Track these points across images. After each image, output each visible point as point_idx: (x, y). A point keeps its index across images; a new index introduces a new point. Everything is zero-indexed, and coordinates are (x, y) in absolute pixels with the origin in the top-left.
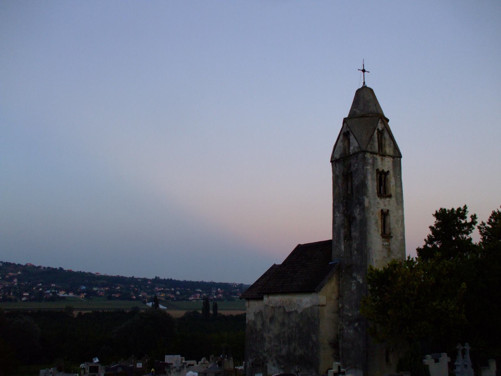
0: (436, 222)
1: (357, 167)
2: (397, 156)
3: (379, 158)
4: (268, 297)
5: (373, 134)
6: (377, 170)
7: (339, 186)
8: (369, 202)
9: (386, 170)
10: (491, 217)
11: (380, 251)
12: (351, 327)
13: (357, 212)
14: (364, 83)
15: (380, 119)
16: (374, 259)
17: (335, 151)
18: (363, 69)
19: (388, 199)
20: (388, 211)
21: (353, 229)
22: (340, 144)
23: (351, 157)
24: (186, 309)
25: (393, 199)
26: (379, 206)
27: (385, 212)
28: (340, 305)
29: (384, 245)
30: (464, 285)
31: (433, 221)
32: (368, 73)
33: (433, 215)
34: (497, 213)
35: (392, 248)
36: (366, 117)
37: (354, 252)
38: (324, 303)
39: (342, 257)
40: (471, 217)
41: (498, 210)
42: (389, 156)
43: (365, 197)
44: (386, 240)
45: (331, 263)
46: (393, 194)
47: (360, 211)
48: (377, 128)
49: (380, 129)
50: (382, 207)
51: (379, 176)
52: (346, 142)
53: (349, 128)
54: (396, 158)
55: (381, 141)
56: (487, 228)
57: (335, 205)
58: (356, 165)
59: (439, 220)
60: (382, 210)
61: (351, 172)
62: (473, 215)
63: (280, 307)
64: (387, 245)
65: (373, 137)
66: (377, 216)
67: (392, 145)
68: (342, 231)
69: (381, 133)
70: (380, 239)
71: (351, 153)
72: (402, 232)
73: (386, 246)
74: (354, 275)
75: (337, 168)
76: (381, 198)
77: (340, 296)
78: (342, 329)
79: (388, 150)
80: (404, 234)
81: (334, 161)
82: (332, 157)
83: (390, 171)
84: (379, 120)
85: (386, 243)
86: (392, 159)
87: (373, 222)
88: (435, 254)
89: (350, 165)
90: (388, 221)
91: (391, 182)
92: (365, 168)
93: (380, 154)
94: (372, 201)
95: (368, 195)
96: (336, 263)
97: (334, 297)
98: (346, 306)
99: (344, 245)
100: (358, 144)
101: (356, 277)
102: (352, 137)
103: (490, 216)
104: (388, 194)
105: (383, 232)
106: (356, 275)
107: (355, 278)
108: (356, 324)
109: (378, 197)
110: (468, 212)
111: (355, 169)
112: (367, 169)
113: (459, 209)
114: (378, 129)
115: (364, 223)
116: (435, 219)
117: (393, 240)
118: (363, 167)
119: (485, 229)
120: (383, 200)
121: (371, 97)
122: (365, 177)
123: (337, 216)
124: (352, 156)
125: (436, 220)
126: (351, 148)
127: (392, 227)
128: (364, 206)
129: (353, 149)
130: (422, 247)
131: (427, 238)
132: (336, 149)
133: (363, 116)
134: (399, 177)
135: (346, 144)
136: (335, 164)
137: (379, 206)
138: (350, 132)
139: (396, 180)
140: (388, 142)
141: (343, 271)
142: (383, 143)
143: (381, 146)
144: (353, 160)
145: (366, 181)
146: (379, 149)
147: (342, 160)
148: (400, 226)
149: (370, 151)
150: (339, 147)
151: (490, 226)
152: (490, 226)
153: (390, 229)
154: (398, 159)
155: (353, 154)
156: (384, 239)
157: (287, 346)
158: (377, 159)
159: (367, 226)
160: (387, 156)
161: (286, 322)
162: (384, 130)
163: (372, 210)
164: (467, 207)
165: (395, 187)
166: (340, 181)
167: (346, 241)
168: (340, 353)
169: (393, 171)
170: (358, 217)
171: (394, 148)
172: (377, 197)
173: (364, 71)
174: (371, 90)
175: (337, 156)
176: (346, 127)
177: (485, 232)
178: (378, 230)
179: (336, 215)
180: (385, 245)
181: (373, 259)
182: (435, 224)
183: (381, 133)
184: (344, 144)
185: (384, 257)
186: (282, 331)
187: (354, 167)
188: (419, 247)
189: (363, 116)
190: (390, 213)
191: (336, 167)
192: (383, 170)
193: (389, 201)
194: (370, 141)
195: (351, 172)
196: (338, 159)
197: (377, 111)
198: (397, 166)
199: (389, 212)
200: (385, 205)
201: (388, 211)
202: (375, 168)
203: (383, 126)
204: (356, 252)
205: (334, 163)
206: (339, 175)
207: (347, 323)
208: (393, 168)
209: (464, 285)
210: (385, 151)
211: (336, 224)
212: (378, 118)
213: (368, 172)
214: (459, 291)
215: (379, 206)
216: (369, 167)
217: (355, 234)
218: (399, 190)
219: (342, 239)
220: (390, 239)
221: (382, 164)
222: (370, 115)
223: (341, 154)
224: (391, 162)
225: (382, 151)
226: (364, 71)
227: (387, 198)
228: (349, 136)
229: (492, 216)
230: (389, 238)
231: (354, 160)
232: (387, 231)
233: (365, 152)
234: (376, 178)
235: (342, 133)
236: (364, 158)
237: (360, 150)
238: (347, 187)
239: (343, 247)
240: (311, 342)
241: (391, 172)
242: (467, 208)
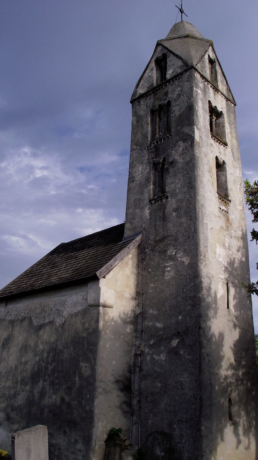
4: (6, 305)
12: (163, 348)
24: (172, 39)
29: (220, 209)
32: (177, 5)
55: (212, 72)
63: (23, 319)
74: (171, 251)
78: (140, 355)
87: (206, 168)
108: (175, 343)
117: (231, 204)
157: (28, 388)
161: (32, 343)
168: (135, 402)
180: (223, 210)
186: (23, 360)
207: (152, 342)
235: (155, 58)
240: (77, 378)
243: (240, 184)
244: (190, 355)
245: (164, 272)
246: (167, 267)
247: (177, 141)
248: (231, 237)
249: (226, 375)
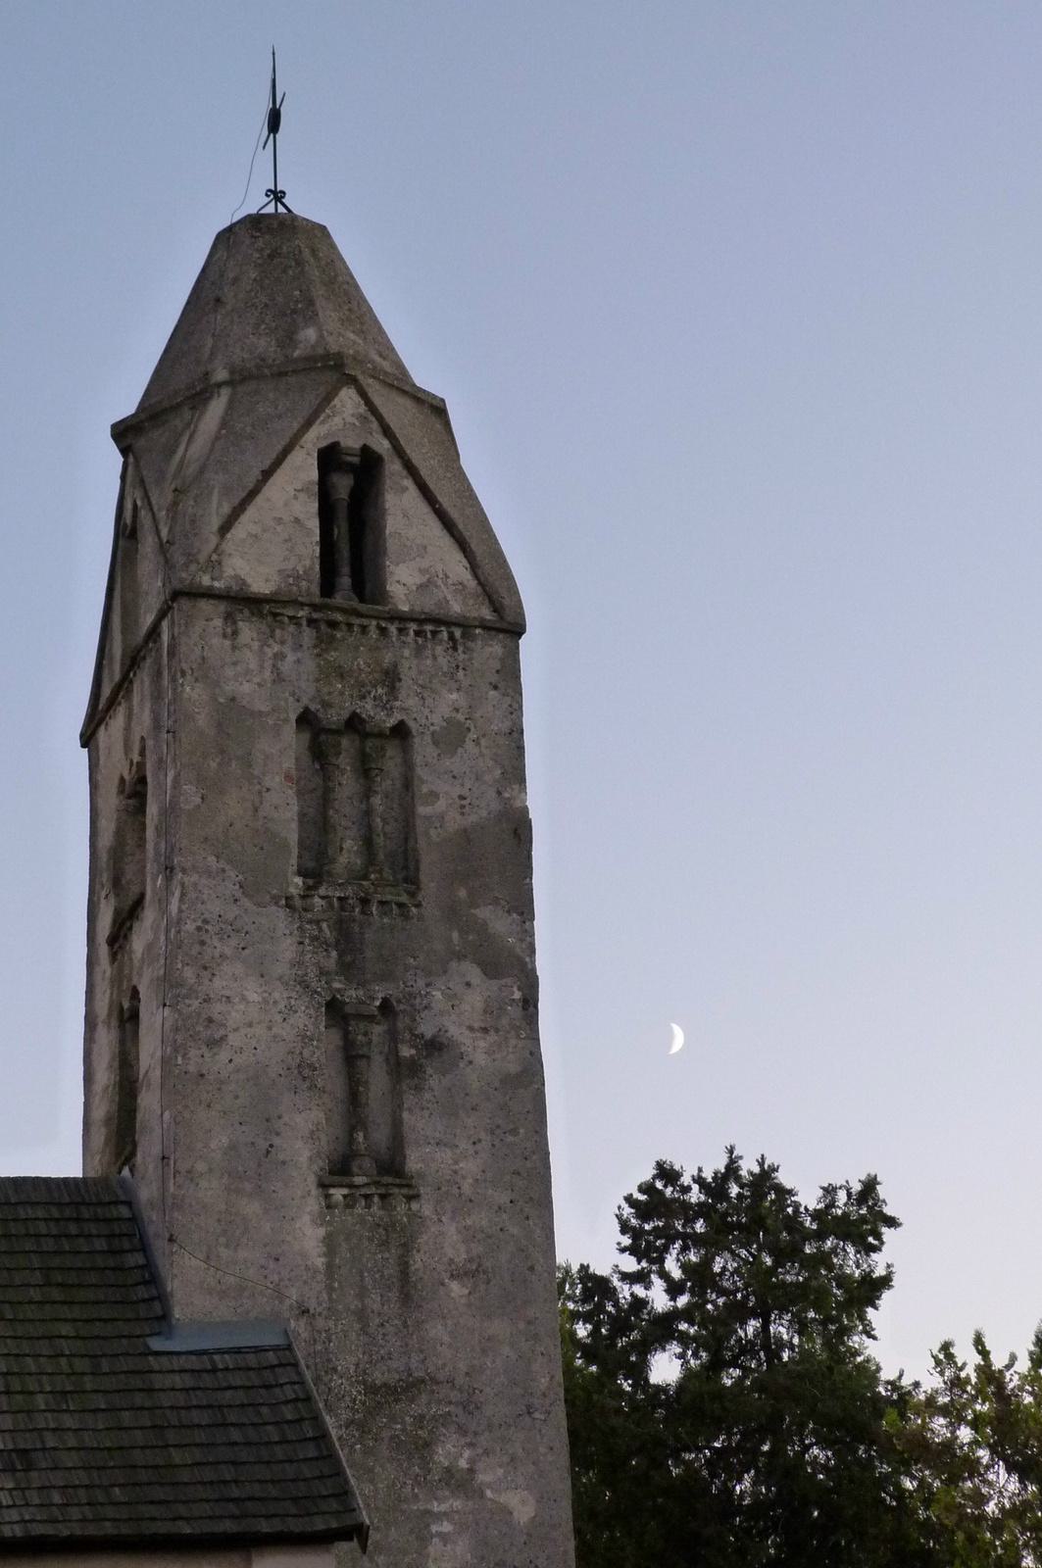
101: (471, 1471)
138: (393, 467)
174: (324, 228)
245: (424, 1539)
246: (439, 1517)
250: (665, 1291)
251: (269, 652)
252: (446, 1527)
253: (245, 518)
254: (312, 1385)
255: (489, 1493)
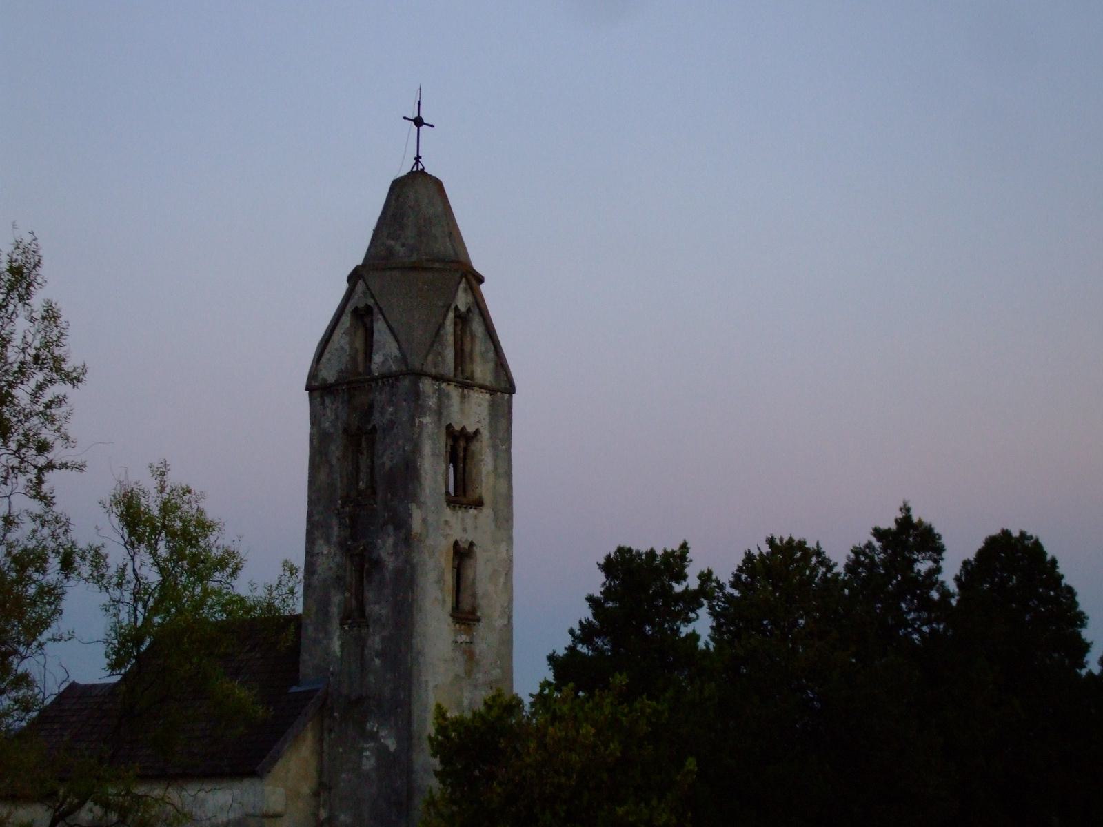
0: (605, 583)
1: (392, 415)
2: (503, 386)
3: (454, 392)
5: (444, 323)
6: (449, 427)
7: (331, 466)
8: (424, 521)
9: (471, 429)
10: (740, 569)
11: (446, 660)
13: (385, 548)
14: (418, 159)
15: (464, 280)
16: (431, 684)
17: (324, 359)
18: (416, 115)
19: (472, 512)
20: (472, 544)
21: (370, 595)
22: (339, 339)
23: (373, 385)
25: (487, 511)
26: (450, 533)
27: (464, 548)
28: (323, 814)
29: (456, 642)
30: (691, 764)
31: (596, 583)
33: (599, 564)
34: (758, 558)
35: (478, 652)
36: (425, 269)
37: (373, 660)
38: (279, 808)
39: (332, 674)
40: (699, 577)
41: (759, 549)
42: (482, 387)
43: (413, 507)
44: (463, 627)
45: (294, 689)
46: (487, 499)
47: (395, 545)
48: (453, 307)
49: (462, 308)
50: (456, 534)
51: (450, 442)
52: (361, 333)
53: (373, 296)
54: (499, 393)
55: (462, 344)
56: (730, 599)
57: (316, 518)
58: (391, 409)
59: (612, 580)
60: (456, 544)
61: (374, 427)
62: (706, 572)
64: (467, 642)
65: (442, 332)
66: (442, 560)
67: (491, 355)
68: (336, 599)
69: (462, 320)
70: (449, 625)
71: (377, 374)
72: (506, 604)
73: (463, 645)
74: (372, 726)
75: (328, 411)
76: (454, 509)
77: (323, 788)
79: (479, 369)
80: (511, 610)
81: (317, 388)
82: (313, 375)
83: (482, 430)
84: (459, 283)
85: (464, 638)
86: (487, 396)
87: (432, 576)
88: (613, 677)
89: (371, 406)
90: (469, 573)
91: (482, 463)
92: (417, 421)
93: (458, 382)
94: (431, 518)
95: (422, 499)
96: (317, 690)
97: (306, 789)
98: (342, 817)
99: (340, 638)
100: (400, 348)
101: (378, 732)
102: (379, 326)
103: (739, 567)
104: (473, 496)
105: (454, 606)
106: (378, 728)
107: (374, 737)
109: (448, 505)
110: (691, 561)
111: (384, 421)
112: (421, 423)
113: (667, 555)
114: (456, 308)
115: (406, 580)
116: (601, 577)
118: (412, 419)
119: (723, 600)
120: (460, 513)
121: (440, 209)
122: (417, 449)
123: (322, 553)
124: (377, 384)
125: (604, 580)
126: (377, 358)
127: (480, 591)
128: (409, 530)
129: (383, 363)
130: (561, 652)
131: (577, 628)
132: (326, 355)
133: (414, 268)
134: (504, 447)
135: (359, 344)
136: (322, 397)
137: (448, 531)
138: (376, 310)
139: (496, 457)
140: (480, 346)
141: (336, 714)
142: (467, 348)
143: (461, 357)
144: (380, 394)
145: (419, 460)
146: (456, 369)
147: (343, 390)
148: (501, 586)
149: (433, 371)
150: (336, 350)
151: (736, 593)
152: (736, 593)
153: (474, 596)
154: (504, 397)
155: (383, 376)
156: (458, 626)
158: (448, 396)
159: (415, 588)
160: (476, 388)
162: (471, 312)
163: (430, 542)
164: (688, 549)
165: (491, 479)
166: (335, 450)
167: (346, 627)
169: (490, 433)
170: (390, 563)
171: (496, 364)
172: (445, 505)
173: (419, 122)
174: (438, 184)
175: (329, 374)
176: (364, 293)
177: (724, 609)
178: (444, 601)
179: (317, 549)
180: (461, 642)
181: (427, 681)
182: (602, 589)
183: (462, 320)
184: (351, 343)
185: (457, 676)
187: (382, 414)
188: (554, 652)
189: (414, 268)
190: (478, 551)
191: (324, 408)
192: (463, 428)
193: (476, 517)
194: (432, 345)
195: (374, 427)
196: (331, 385)
197: (456, 254)
198: (502, 414)
199: (475, 548)
200: (464, 530)
201: (472, 544)
202: (443, 420)
203: (470, 299)
204: (377, 661)
205: (316, 394)
206: (332, 431)
208: (491, 425)
209: (691, 764)
210: (472, 372)
211: (316, 577)
212: (459, 275)
213: (425, 435)
214: (679, 778)
215: (448, 531)
216: (427, 420)
217: (378, 609)
218: (502, 484)
219: (335, 623)
220: (474, 625)
221: (462, 411)
222: (437, 265)
223: (341, 371)
224: (485, 404)
225: (463, 372)
226: (419, 122)
227: (471, 508)
228: (372, 321)
229: (744, 565)
230: (471, 623)
231: (384, 396)
232: (466, 605)
233: (419, 375)
234: (443, 450)
235: (349, 309)
236: (417, 394)
237: (404, 368)
238: (357, 469)
239: (336, 645)
241: (485, 434)
242: (690, 550)
243: (506, 574)
244: (103, 576)
245: (361, 757)
246: (366, 749)
247: (386, 523)
248: (476, 687)
249: (59, 598)
250: (749, 557)
251: (334, 407)
252: (368, 753)
253: (326, 352)
254: (360, 377)
255: (382, 740)
